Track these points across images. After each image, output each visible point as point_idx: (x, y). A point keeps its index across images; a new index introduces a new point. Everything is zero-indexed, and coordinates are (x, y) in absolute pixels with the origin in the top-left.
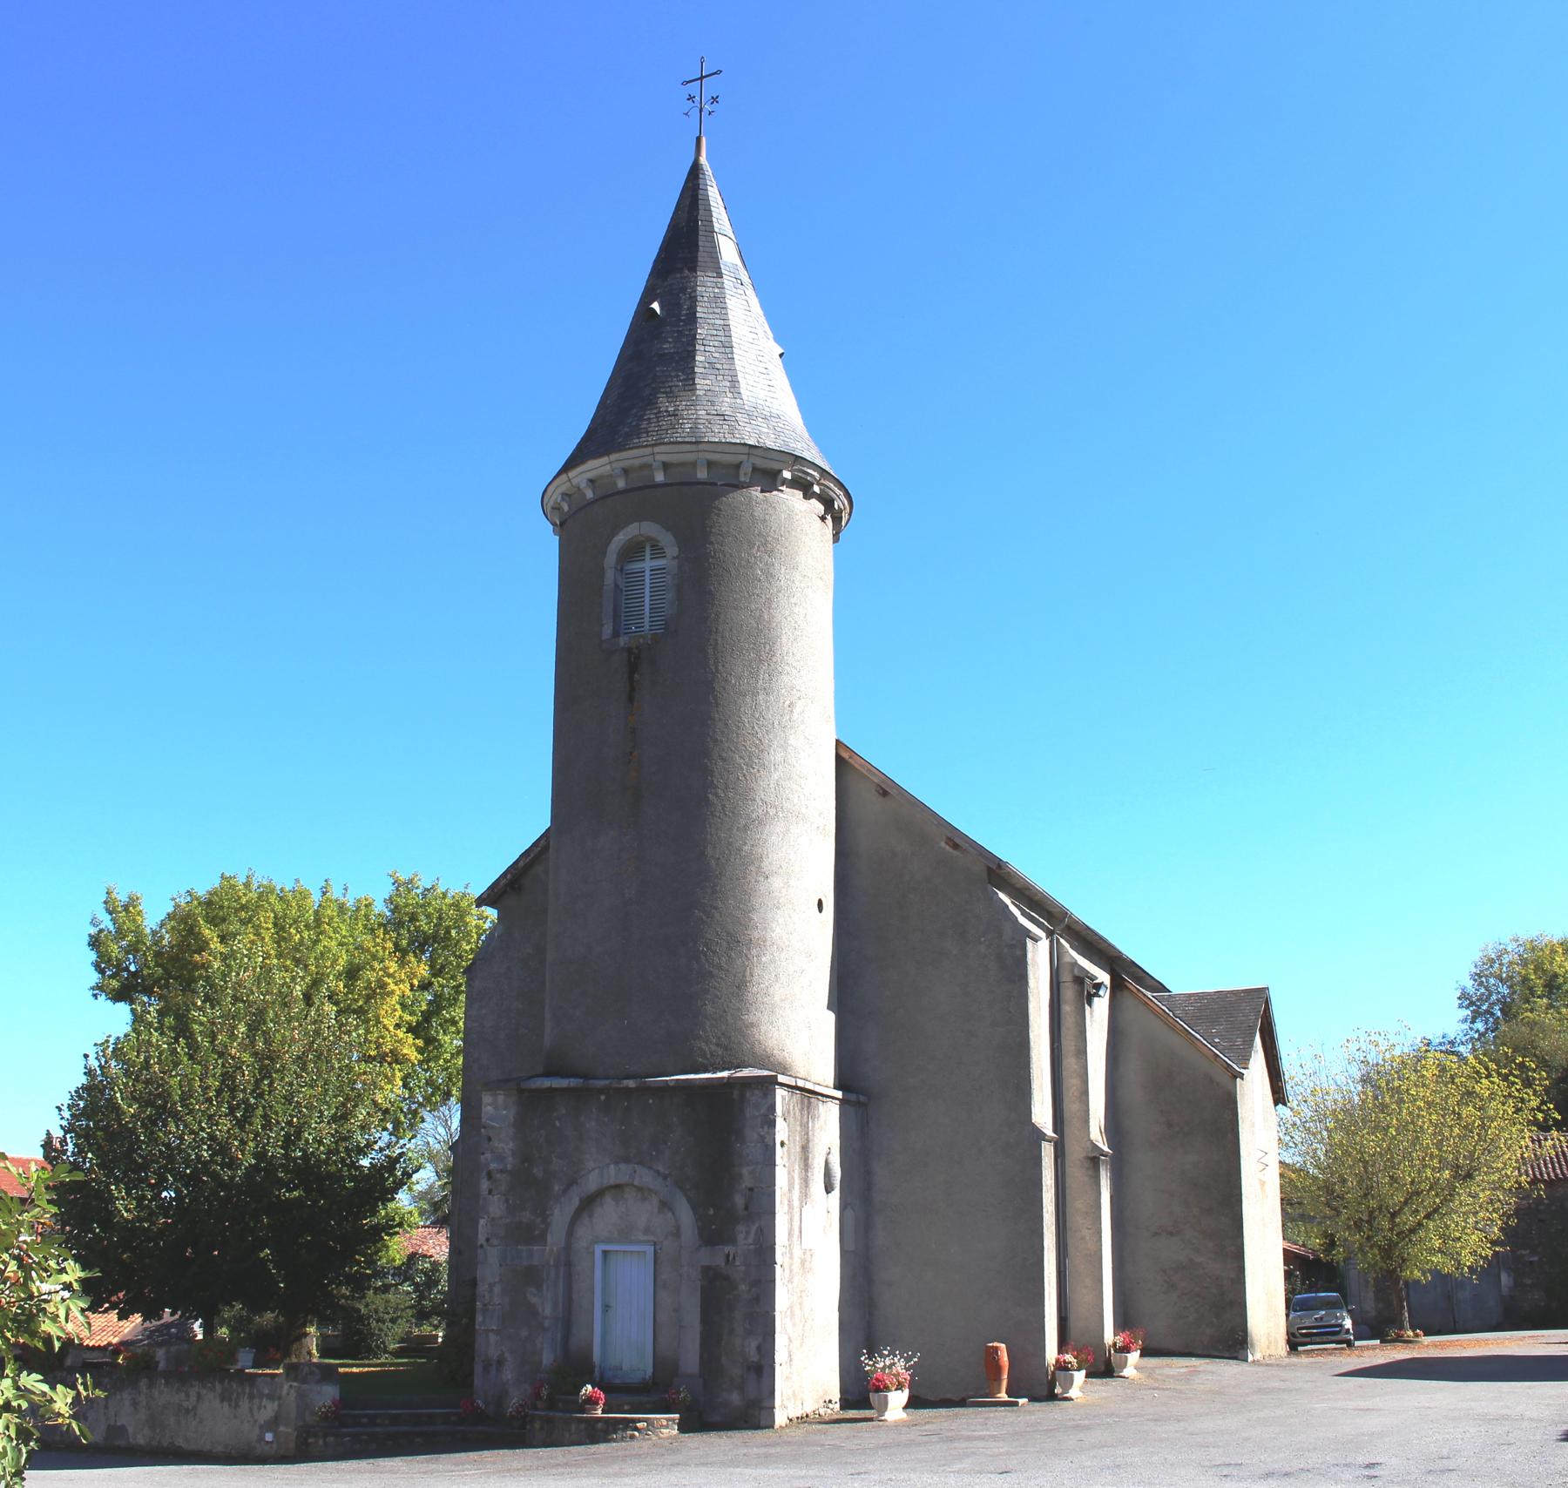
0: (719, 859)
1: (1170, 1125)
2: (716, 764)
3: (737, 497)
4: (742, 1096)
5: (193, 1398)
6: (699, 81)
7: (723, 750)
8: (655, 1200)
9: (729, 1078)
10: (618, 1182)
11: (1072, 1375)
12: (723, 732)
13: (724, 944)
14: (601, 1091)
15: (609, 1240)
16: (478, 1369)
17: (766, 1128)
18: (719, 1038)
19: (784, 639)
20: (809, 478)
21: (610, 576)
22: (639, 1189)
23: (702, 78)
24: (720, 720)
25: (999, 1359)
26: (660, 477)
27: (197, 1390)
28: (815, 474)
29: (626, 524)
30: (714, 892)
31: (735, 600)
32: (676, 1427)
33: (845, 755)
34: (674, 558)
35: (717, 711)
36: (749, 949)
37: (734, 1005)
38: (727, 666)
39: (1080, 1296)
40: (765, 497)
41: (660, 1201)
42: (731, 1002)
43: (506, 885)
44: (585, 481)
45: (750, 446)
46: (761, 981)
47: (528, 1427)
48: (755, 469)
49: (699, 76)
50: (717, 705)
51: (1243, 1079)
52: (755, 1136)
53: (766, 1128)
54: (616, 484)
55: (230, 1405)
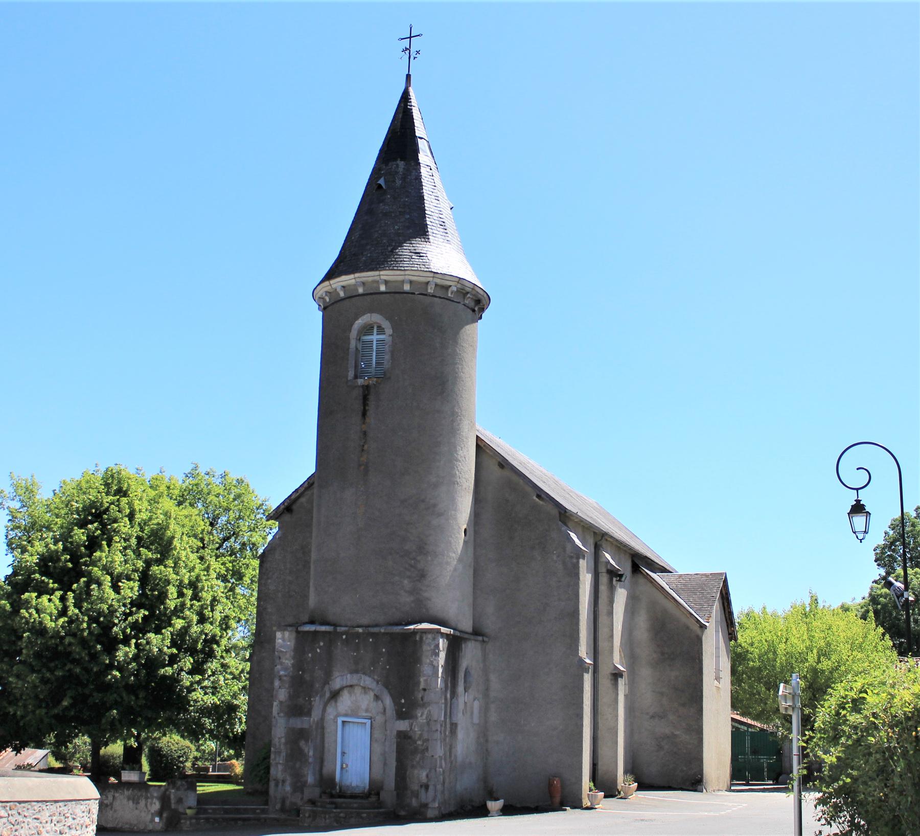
1: (663, 654)
4: (421, 638)
5: (110, 798)
6: (412, 35)
8: (372, 694)
9: (414, 629)
10: (351, 684)
14: (343, 633)
15: (346, 715)
16: (272, 784)
17: (434, 657)
21: (353, 343)
22: (364, 688)
23: (410, 37)
26: (383, 288)
27: (112, 793)
29: (364, 314)
33: (479, 443)
34: (390, 335)
39: (603, 751)
41: (375, 694)
43: (284, 509)
44: (340, 287)
45: (435, 273)
47: (301, 816)
48: (436, 285)
49: (409, 36)
52: (428, 661)
53: (434, 657)
54: (357, 290)
55: (133, 803)
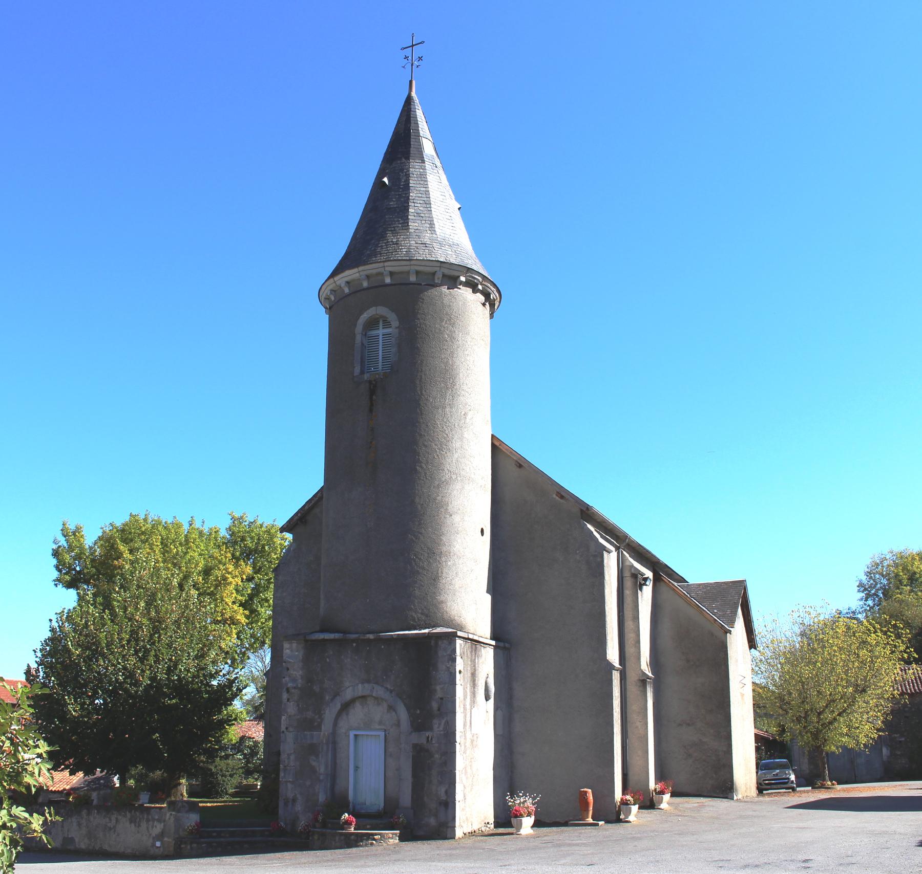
0: (423, 504)
1: (688, 661)
2: (421, 449)
3: (434, 292)
4: (436, 644)
5: (114, 821)
7: (425, 440)
8: (385, 705)
9: (429, 633)
10: (364, 694)
11: (630, 808)
12: (425, 430)
13: (426, 555)
14: (353, 641)
15: (358, 729)
16: (281, 804)
17: (450, 662)
18: (423, 610)
19: (461, 375)
20: (476, 281)
21: (359, 338)
22: (376, 698)
23: (413, 46)
24: (423, 423)
25: (587, 799)
26: (388, 280)
27: (116, 816)
28: (479, 278)
29: (368, 308)
30: (420, 524)
31: (432, 352)
32: (398, 838)
33: (497, 443)
34: (396, 328)
35: (422, 418)
36: (440, 558)
37: (432, 590)
38: (427, 391)
39: (635, 761)
40: (450, 292)
41: (388, 705)
42: (430, 588)
43: (298, 520)
44: (344, 282)
45: (441, 262)
46: (447, 576)
47: (310, 838)
48: (444, 276)
49: (411, 45)
50: (422, 414)
51: (731, 634)
52: (444, 667)
53: (450, 662)
54: (362, 284)
55: (135, 825)
